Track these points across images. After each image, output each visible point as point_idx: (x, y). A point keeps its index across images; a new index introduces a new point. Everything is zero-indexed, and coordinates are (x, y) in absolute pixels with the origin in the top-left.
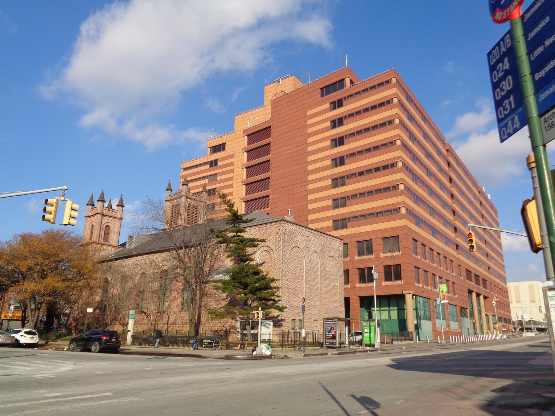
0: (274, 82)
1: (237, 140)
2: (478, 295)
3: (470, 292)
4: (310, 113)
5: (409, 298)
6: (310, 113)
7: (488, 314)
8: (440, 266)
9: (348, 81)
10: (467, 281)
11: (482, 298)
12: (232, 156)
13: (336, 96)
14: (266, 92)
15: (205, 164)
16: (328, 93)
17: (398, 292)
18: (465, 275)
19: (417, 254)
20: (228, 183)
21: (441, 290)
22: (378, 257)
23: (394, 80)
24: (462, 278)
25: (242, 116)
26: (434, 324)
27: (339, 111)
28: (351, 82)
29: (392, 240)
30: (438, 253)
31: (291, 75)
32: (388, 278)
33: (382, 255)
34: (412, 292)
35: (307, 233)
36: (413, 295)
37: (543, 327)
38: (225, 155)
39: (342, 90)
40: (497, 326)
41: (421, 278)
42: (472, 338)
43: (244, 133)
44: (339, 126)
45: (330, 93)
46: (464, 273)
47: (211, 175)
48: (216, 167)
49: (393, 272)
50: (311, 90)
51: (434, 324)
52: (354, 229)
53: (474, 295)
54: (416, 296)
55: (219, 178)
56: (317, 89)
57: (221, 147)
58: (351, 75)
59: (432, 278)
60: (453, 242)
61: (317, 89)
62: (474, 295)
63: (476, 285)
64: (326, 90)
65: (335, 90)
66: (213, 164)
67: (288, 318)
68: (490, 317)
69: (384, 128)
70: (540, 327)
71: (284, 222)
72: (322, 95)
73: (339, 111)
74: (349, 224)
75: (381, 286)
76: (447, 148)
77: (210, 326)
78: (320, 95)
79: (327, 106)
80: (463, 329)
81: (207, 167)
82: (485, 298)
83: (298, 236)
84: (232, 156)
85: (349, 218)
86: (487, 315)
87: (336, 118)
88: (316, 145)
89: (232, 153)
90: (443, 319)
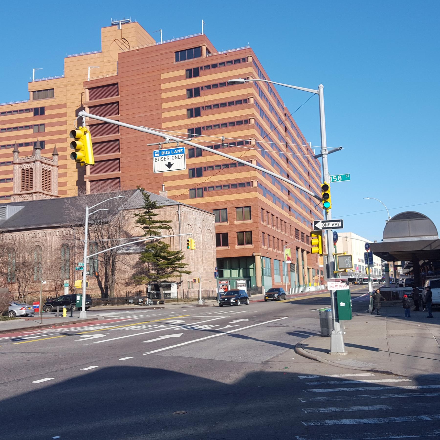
0: (113, 25)
1: (69, 88)
2: (303, 251)
3: (297, 248)
4: (164, 76)
5: (258, 259)
6: (164, 76)
7: (309, 268)
8: (278, 229)
9: (204, 49)
10: (296, 239)
11: (305, 252)
12: (64, 106)
13: (192, 63)
14: (102, 35)
15: (27, 110)
16: (183, 59)
17: (250, 255)
18: (294, 234)
19: (263, 221)
20: (61, 136)
21: (286, 253)
22: (232, 224)
23: (250, 59)
24: (292, 237)
25: (74, 59)
26: (273, 279)
27: (195, 81)
28: (208, 52)
29: (246, 210)
30: (272, 215)
31: (134, 22)
32: (241, 243)
33: (236, 222)
34: (260, 254)
35: (194, 212)
36: (261, 256)
37: (353, 277)
38: (54, 104)
39: (199, 58)
40: (316, 278)
41: (266, 241)
42: (299, 290)
43: (84, 85)
44: (195, 96)
45: (185, 59)
46: (294, 233)
47: (37, 125)
48: (42, 116)
49: (246, 238)
50: (164, 52)
51: (273, 279)
52: (210, 198)
53: (300, 250)
54: (262, 257)
55: (47, 130)
56: (172, 52)
57: (48, 93)
58: (207, 44)
59: (281, 244)
60: (287, 205)
61: (172, 52)
62: (300, 250)
63: (302, 242)
64: (182, 55)
65: (190, 57)
66: (39, 112)
67: (186, 280)
68: (311, 270)
69: (240, 106)
70: (351, 277)
71: (181, 206)
72: (177, 60)
73: (195, 81)
74: (205, 193)
75: (235, 249)
76: (285, 112)
77: (120, 290)
78: (174, 59)
79: (183, 72)
80: (292, 282)
81: (31, 114)
82: (308, 253)
83: (189, 216)
84: (64, 106)
85: (205, 188)
86: (308, 269)
87: (193, 87)
88: (172, 112)
89: (64, 102)
90: (287, 276)
